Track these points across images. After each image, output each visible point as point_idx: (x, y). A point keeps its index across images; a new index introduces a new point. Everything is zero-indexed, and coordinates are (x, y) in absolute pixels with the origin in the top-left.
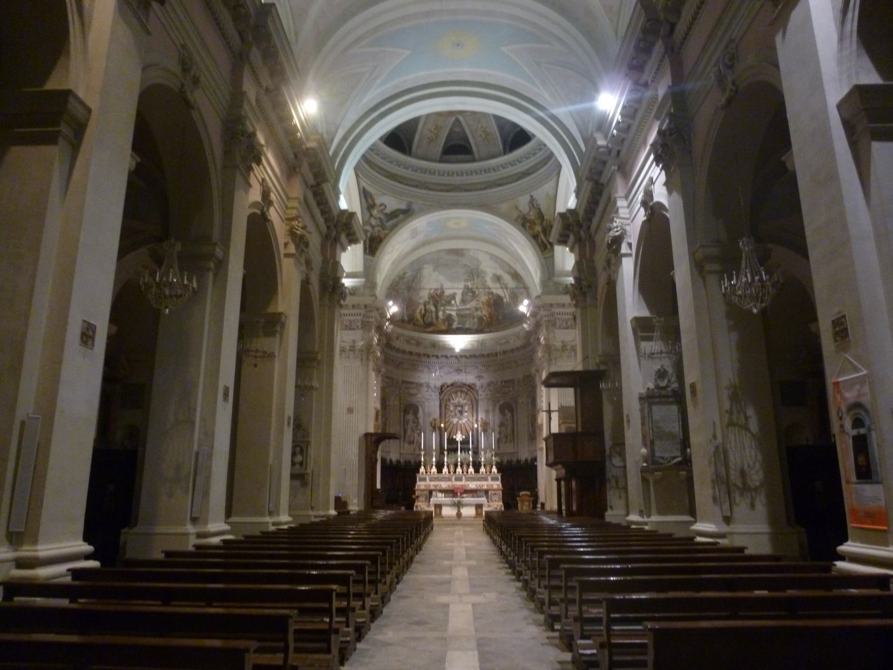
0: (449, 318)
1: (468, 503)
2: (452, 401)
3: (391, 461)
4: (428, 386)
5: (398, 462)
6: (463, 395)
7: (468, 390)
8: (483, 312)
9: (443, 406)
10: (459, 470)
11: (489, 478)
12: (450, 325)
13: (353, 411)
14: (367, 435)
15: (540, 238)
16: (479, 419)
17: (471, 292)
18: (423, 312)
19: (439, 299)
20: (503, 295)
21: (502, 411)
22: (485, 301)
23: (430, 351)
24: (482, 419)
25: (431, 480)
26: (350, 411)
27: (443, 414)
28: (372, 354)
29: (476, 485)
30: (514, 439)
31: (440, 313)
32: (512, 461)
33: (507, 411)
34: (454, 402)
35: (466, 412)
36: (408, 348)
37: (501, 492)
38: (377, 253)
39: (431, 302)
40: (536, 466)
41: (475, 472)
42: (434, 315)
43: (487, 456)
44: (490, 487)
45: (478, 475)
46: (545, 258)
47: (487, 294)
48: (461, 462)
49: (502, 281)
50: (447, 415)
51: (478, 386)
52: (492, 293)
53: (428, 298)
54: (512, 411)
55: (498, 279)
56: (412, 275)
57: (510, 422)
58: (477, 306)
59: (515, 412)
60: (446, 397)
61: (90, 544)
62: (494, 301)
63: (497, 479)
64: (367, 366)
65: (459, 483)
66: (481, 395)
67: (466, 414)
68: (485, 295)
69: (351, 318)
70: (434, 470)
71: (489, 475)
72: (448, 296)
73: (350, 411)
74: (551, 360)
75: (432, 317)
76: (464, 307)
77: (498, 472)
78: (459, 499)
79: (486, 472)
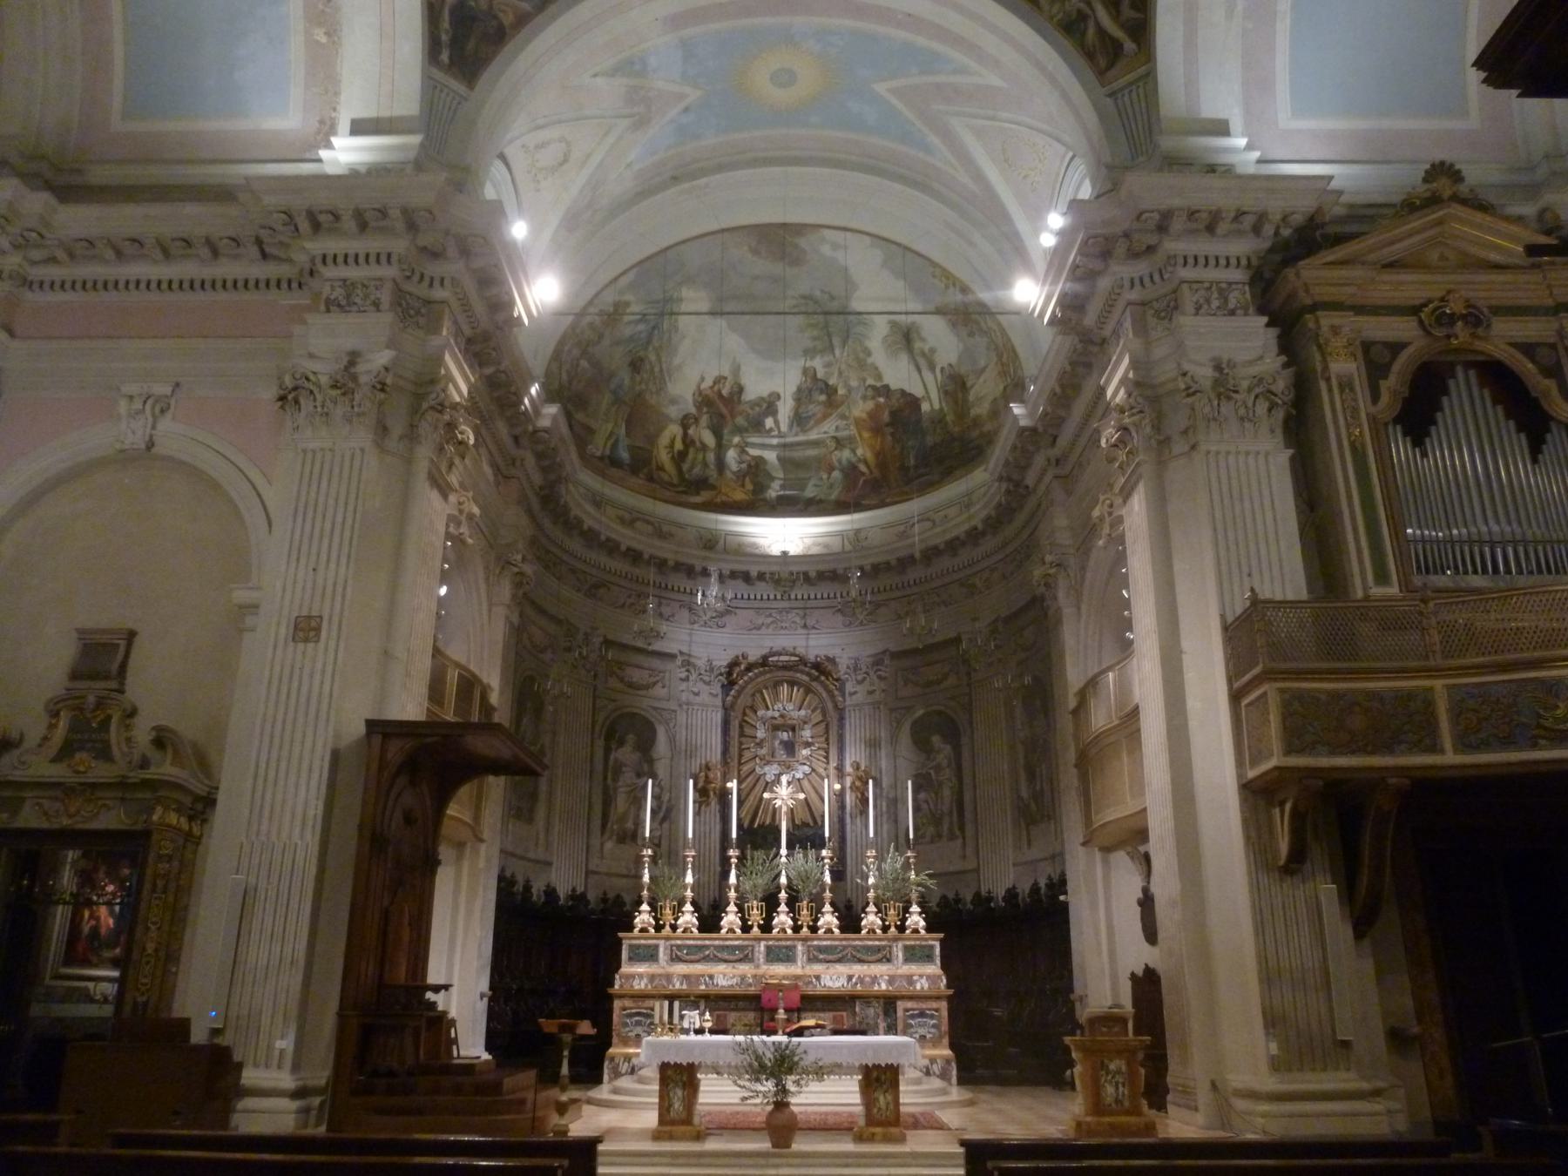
0: (756, 469)
1: (827, 1060)
2: (760, 713)
3: (551, 893)
4: (688, 664)
5: (578, 898)
6: (797, 693)
7: (816, 679)
8: (859, 452)
9: (735, 728)
10: (783, 919)
11: (899, 953)
12: (760, 488)
13: (318, 629)
14: (379, 729)
15: (1091, 32)
16: (848, 769)
17: (822, 392)
18: (679, 446)
19: (724, 411)
20: (918, 391)
21: (921, 742)
22: (864, 415)
23: (695, 557)
24: (857, 766)
25: (675, 959)
26: (306, 629)
27: (734, 750)
28: (431, 416)
29: (850, 978)
30: (962, 828)
31: (731, 455)
32: (958, 900)
33: (936, 740)
34: (770, 713)
35: (808, 745)
36: (627, 537)
37: (943, 1005)
38: (485, 77)
39: (704, 420)
40: (1065, 907)
41: (843, 929)
42: (711, 457)
43: (886, 866)
44: (901, 987)
45: (854, 940)
46: (1112, 95)
47: (870, 393)
48: (790, 887)
49: (917, 345)
50: (747, 755)
51: (842, 668)
52: (885, 391)
53: (695, 401)
54: (952, 734)
55: (906, 338)
56: (644, 317)
57: (947, 773)
58: (839, 434)
59: (965, 740)
60: (744, 701)
61: (490, 1054)
62: (893, 414)
63: (925, 956)
64: (409, 461)
65: (780, 969)
66: (852, 694)
67: (805, 752)
68: (864, 398)
69: (352, 273)
70: (688, 918)
71: (896, 940)
72: (757, 402)
73: (306, 629)
74: (1165, 442)
75: (705, 465)
76: (801, 438)
77: (929, 929)
78: (781, 1038)
79: (885, 929)
